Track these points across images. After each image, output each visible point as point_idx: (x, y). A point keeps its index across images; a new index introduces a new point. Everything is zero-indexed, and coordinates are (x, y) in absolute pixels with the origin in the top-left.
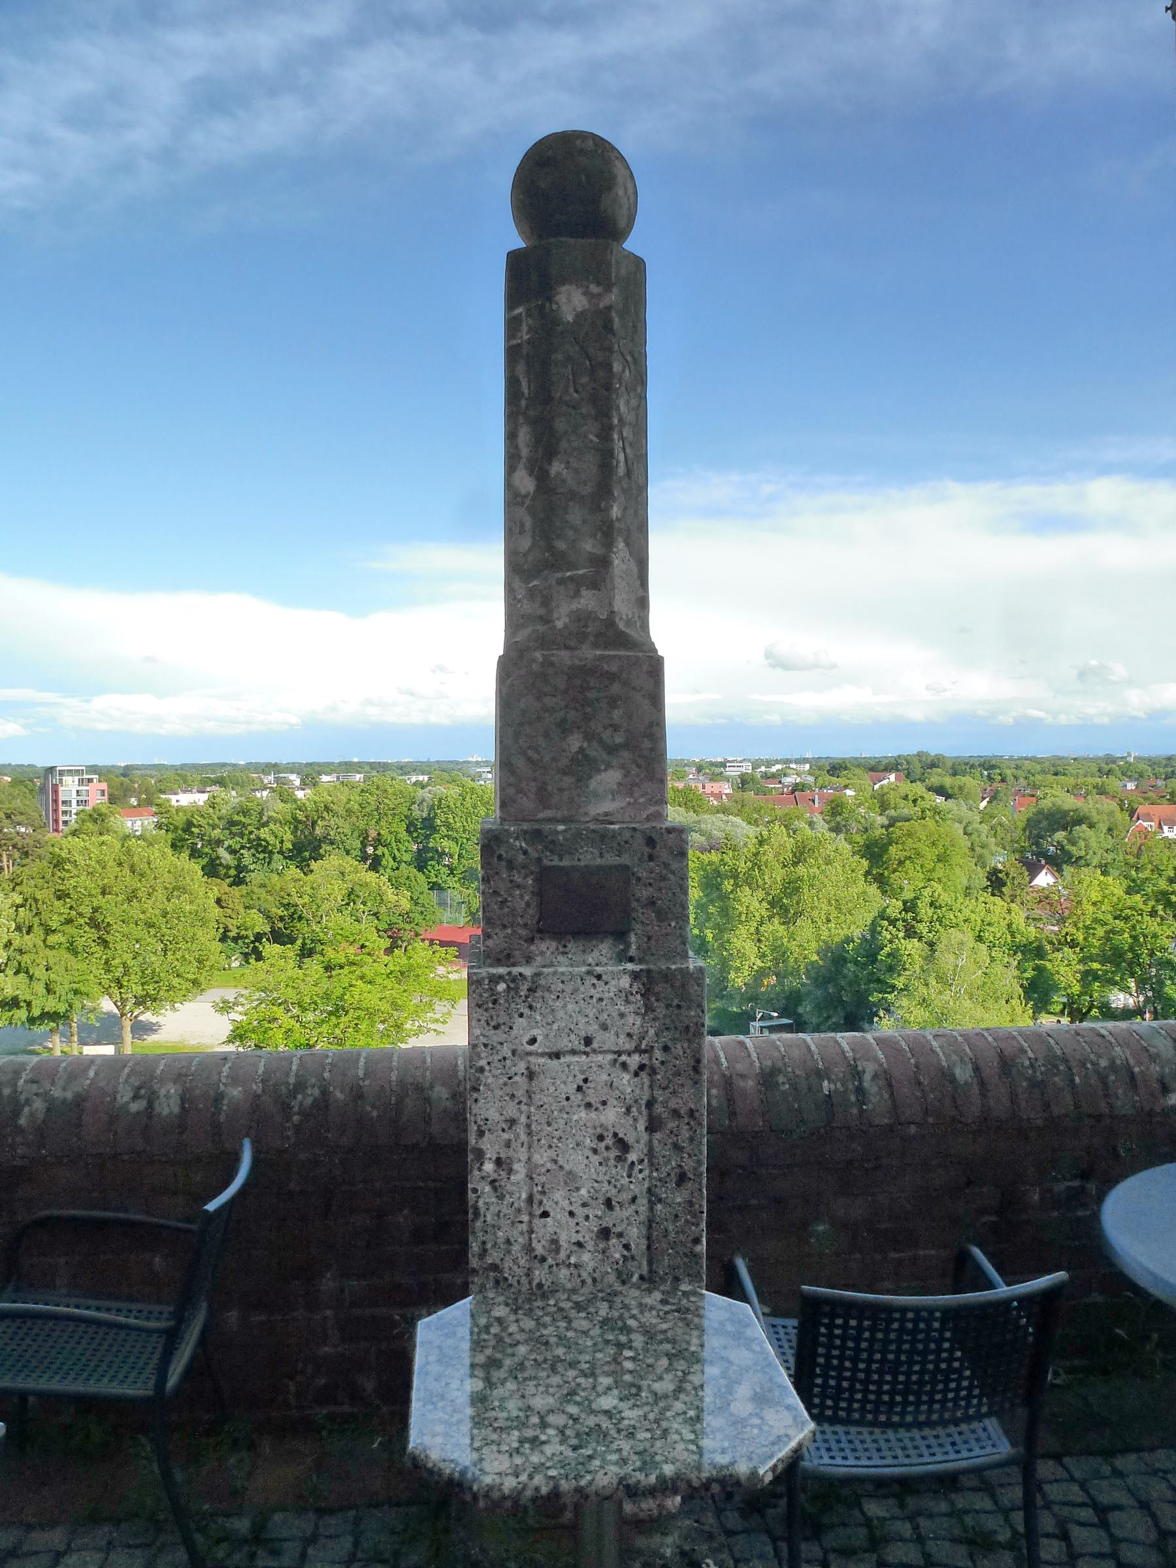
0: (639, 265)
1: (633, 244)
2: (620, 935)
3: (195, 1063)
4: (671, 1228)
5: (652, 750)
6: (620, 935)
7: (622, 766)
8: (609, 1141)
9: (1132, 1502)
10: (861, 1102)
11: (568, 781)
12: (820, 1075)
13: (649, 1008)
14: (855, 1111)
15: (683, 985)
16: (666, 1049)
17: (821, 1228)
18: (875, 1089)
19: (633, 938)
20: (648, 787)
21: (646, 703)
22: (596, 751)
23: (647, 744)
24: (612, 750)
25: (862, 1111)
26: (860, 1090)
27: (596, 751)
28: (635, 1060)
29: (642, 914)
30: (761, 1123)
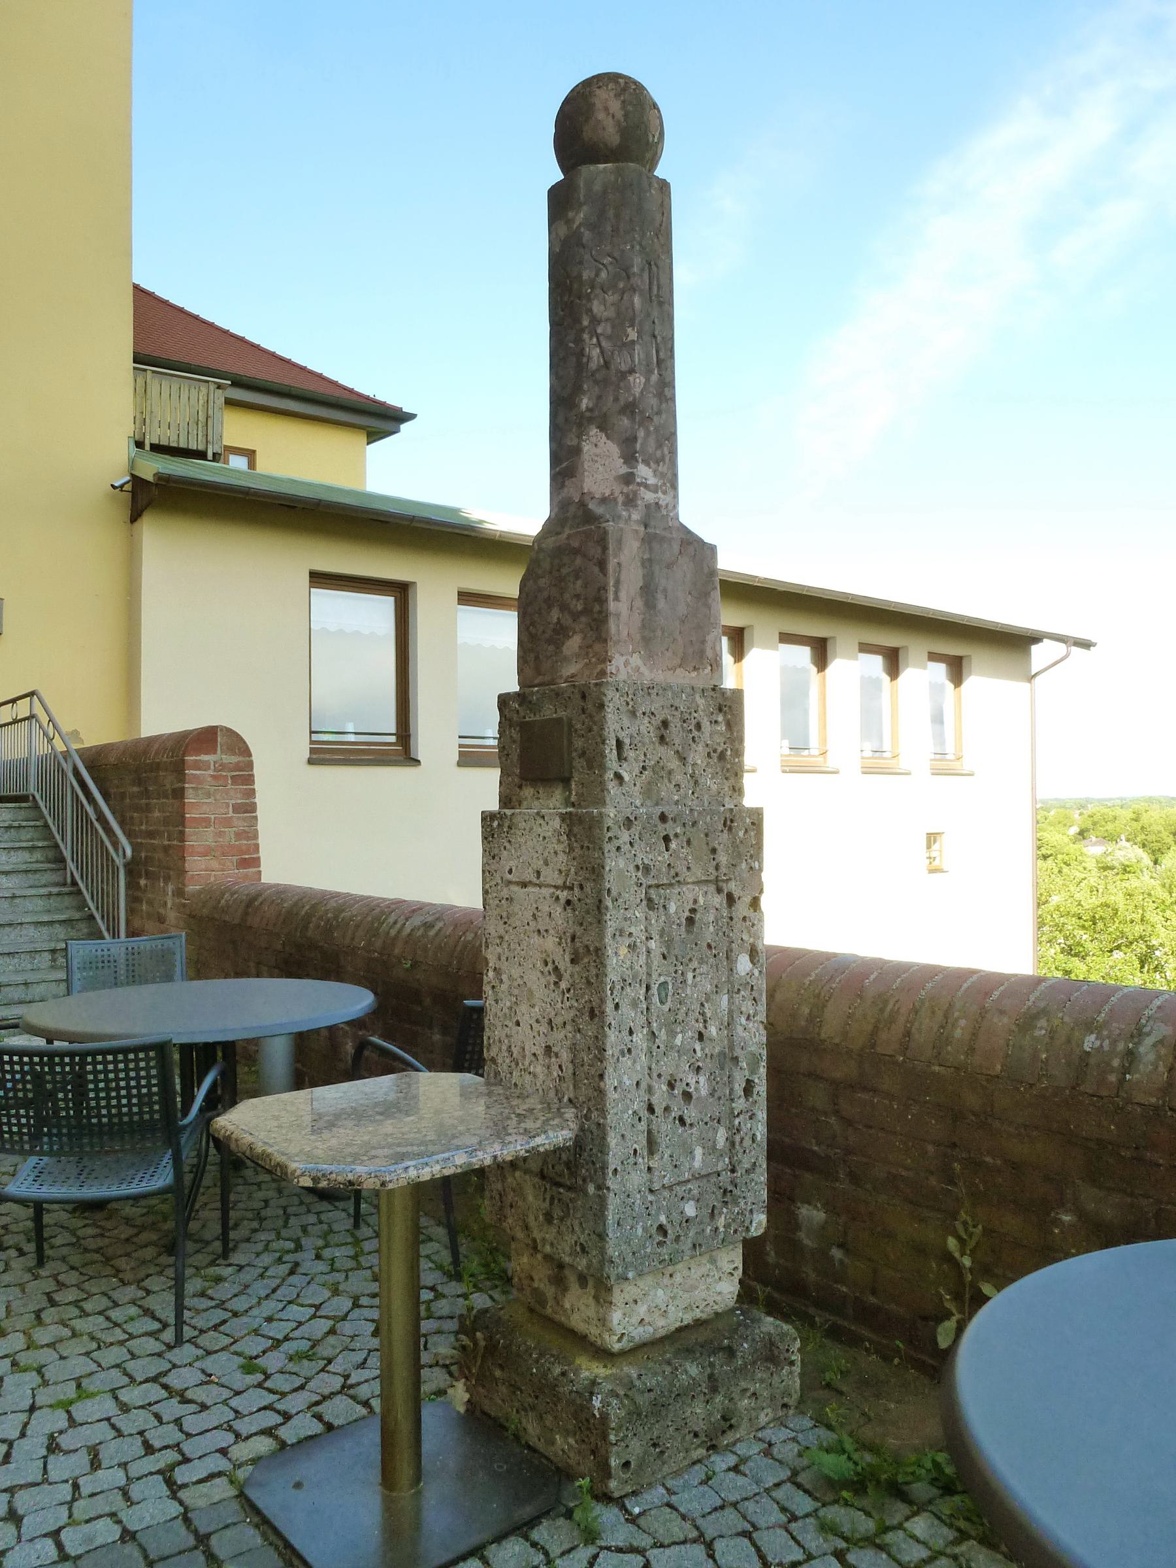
0: (664, 186)
1: (660, 172)
2: (566, 781)
3: (965, 985)
4: (585, 1059)
5: (600, 612)
6: (566, 781)
7: (582, 631)
8: (550, 967)
9: (276, 1317)
10: (1125, 1070)
11: (551, 648)
12: (1089, 1026)
13: (571, 849)
14: (1113, 1078)
15: (590, 828)
16: (581, 887)
17: (1066, 1218)
18: (1151, 1057)
19: (573, 784)
20: (597, 647)
21: (596, 569)
22: (567, 621)
23: (597, 608)
24: (576, 616)
25: (1122, 1081)
26: (1131, 1055)
27: (567, 621)
28: (564, 895)
29: (579, 763)
30: (999, 1067)
